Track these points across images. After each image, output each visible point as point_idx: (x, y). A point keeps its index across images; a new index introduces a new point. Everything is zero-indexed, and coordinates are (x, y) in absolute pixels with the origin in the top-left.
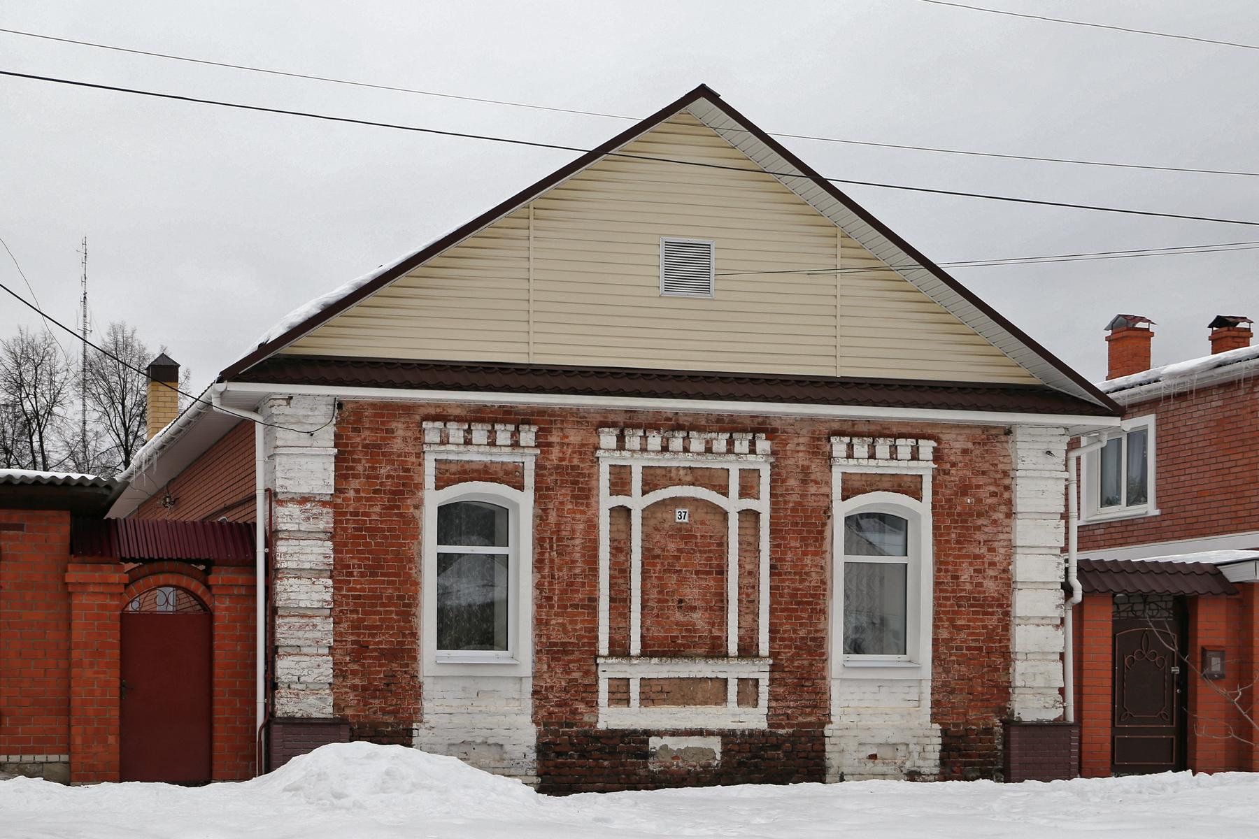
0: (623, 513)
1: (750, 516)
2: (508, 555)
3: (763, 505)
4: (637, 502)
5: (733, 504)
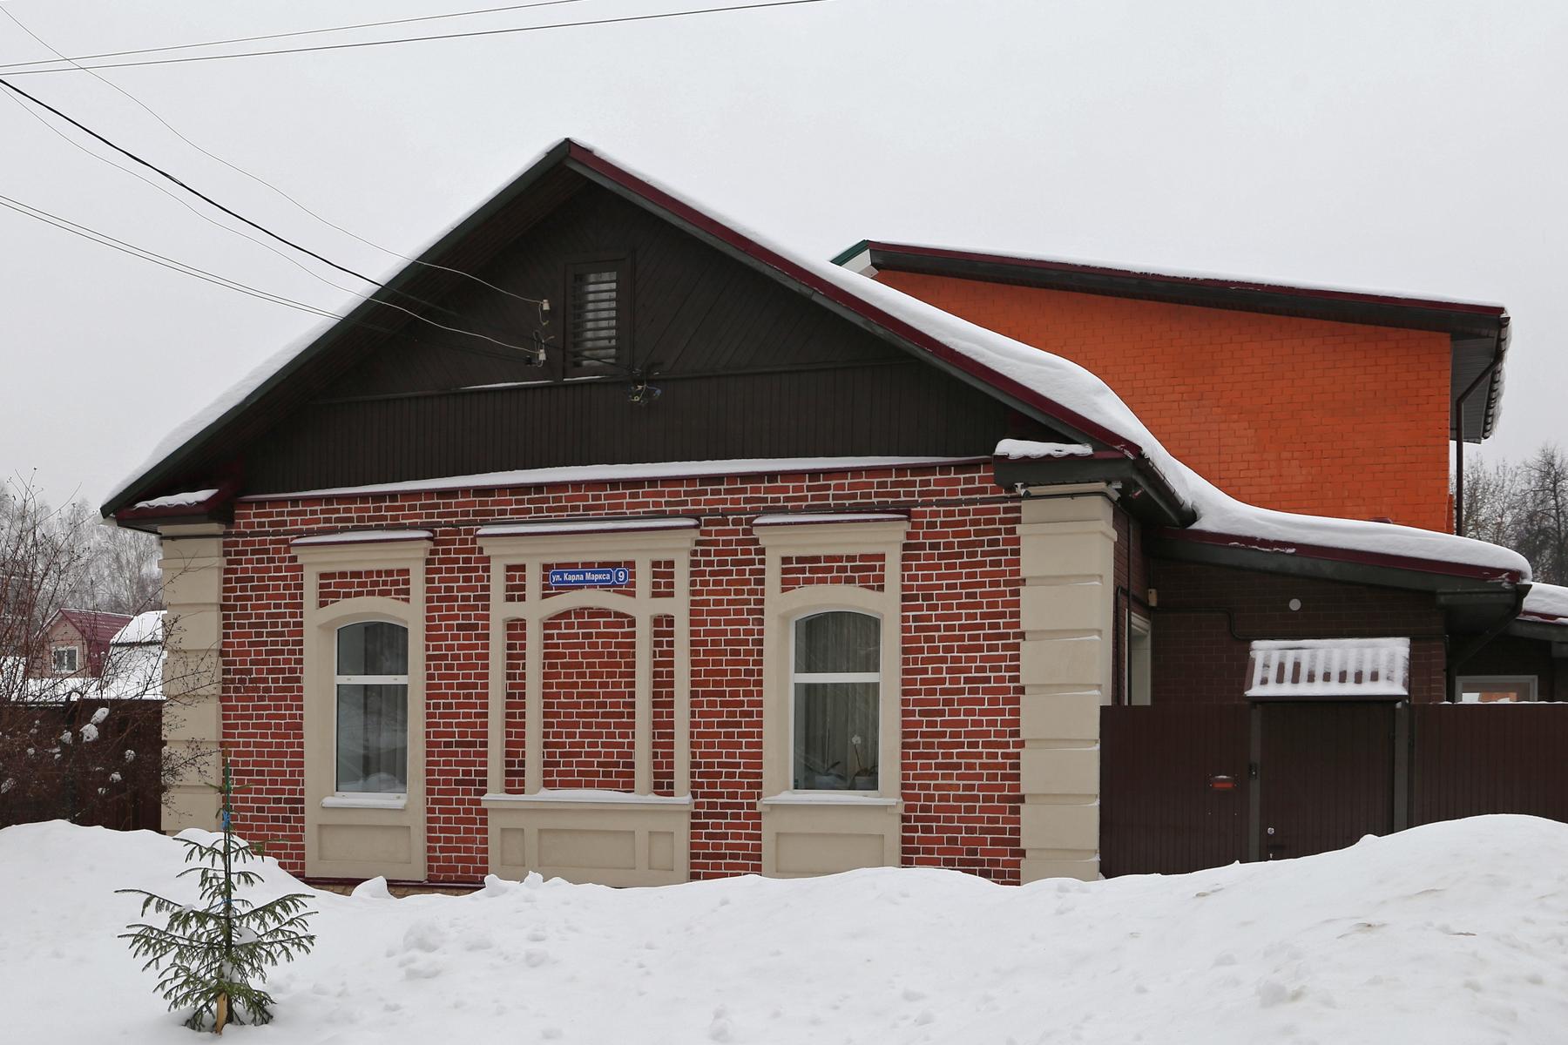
0: (516, 628)
1: (663, 625)
3: (678, 606)
4: (535, 610)
5: (643, 607)
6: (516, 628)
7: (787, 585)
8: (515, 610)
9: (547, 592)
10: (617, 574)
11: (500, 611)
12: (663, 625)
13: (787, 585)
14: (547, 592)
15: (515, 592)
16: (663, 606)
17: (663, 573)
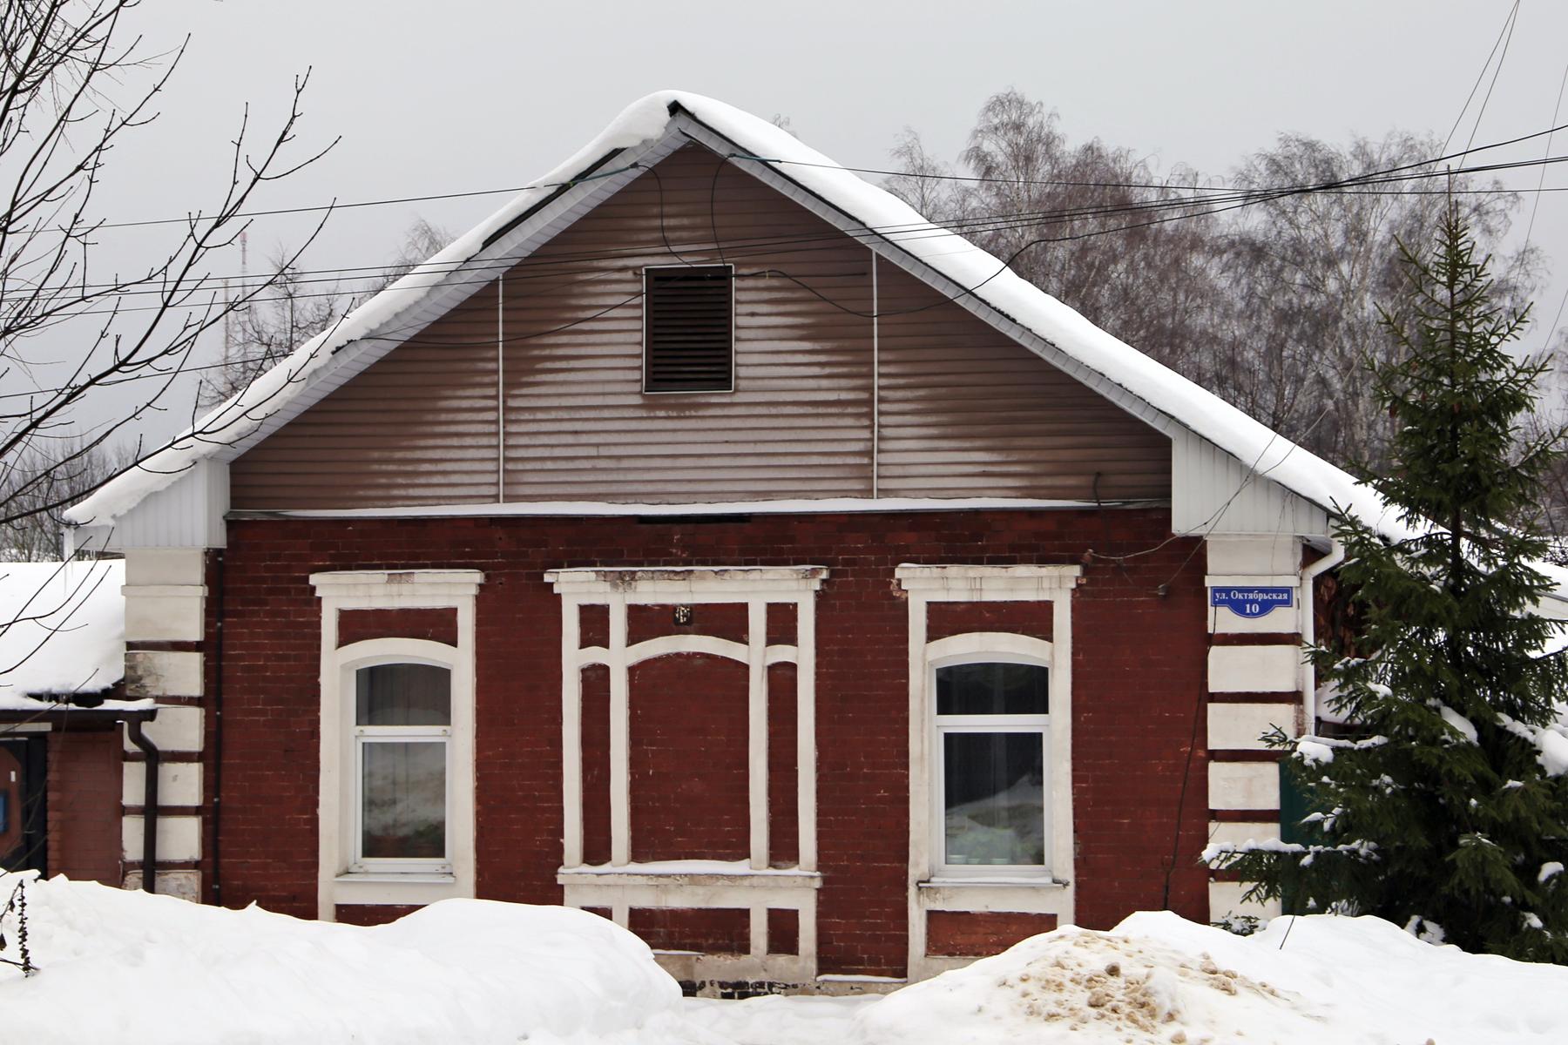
0: (595, 679)
1: (782, 679)
2: (946, 863)
3: (803, 654)
4: (620, 656)
5: (756, 654)
6: (595, 679)
7: (934, 633)
8: (595, 655)
9: (633, 638)
10: (731, 621)
11: (574, 658)
12: (782, 679)
13: (934, 633)
14: (633, 638)
15: (594, 624)
16: (782, 653)
17: (782, 623)
